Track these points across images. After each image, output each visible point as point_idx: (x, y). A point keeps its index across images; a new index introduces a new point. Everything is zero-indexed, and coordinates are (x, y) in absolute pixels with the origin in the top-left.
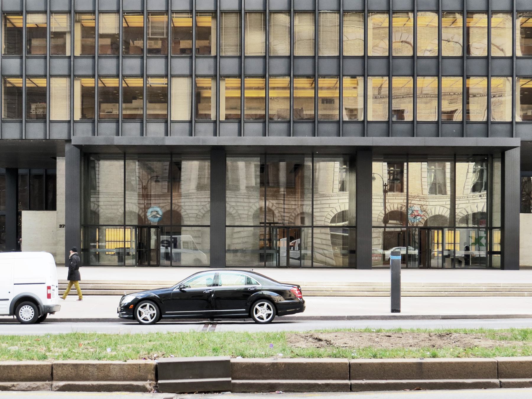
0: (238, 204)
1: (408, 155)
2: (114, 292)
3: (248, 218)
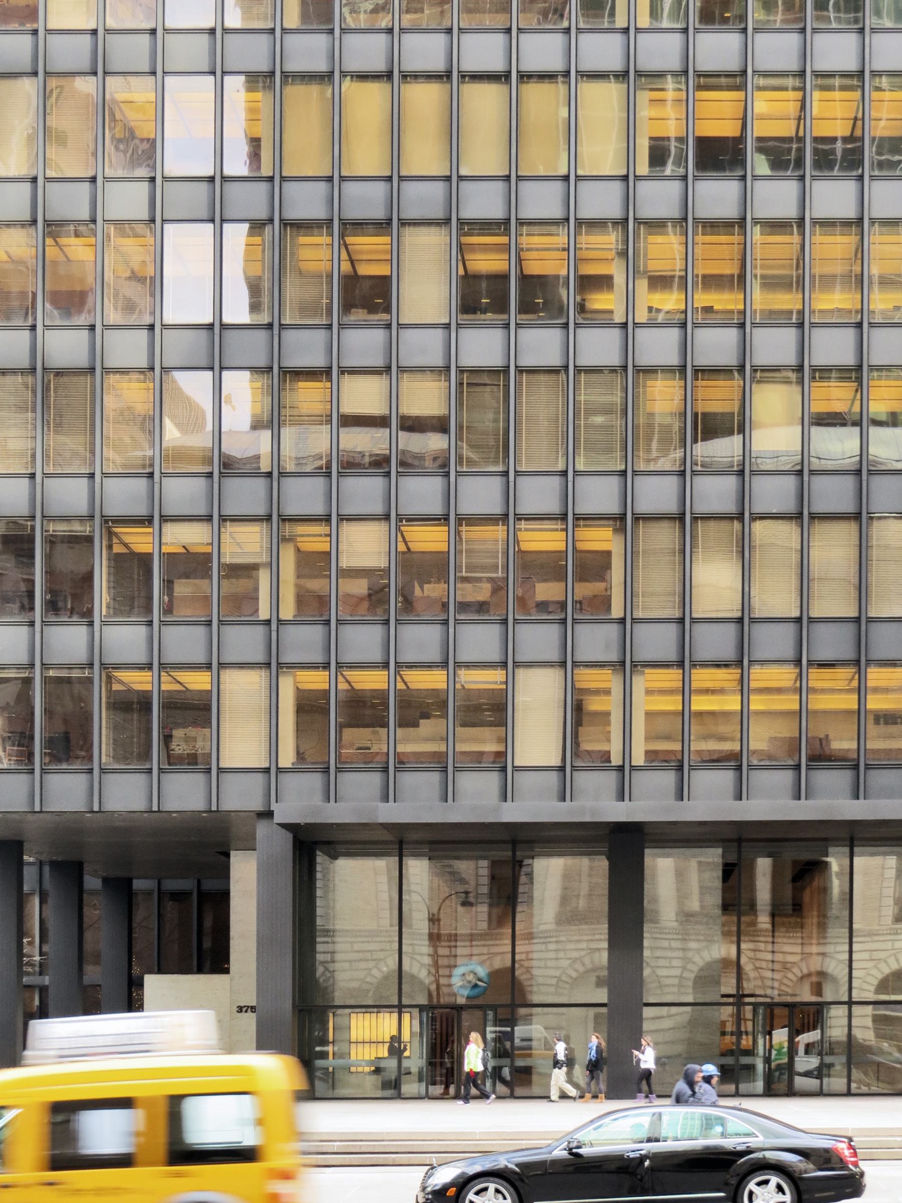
0: (659, 953)
2: (394, 1159)
3: (680, 986)
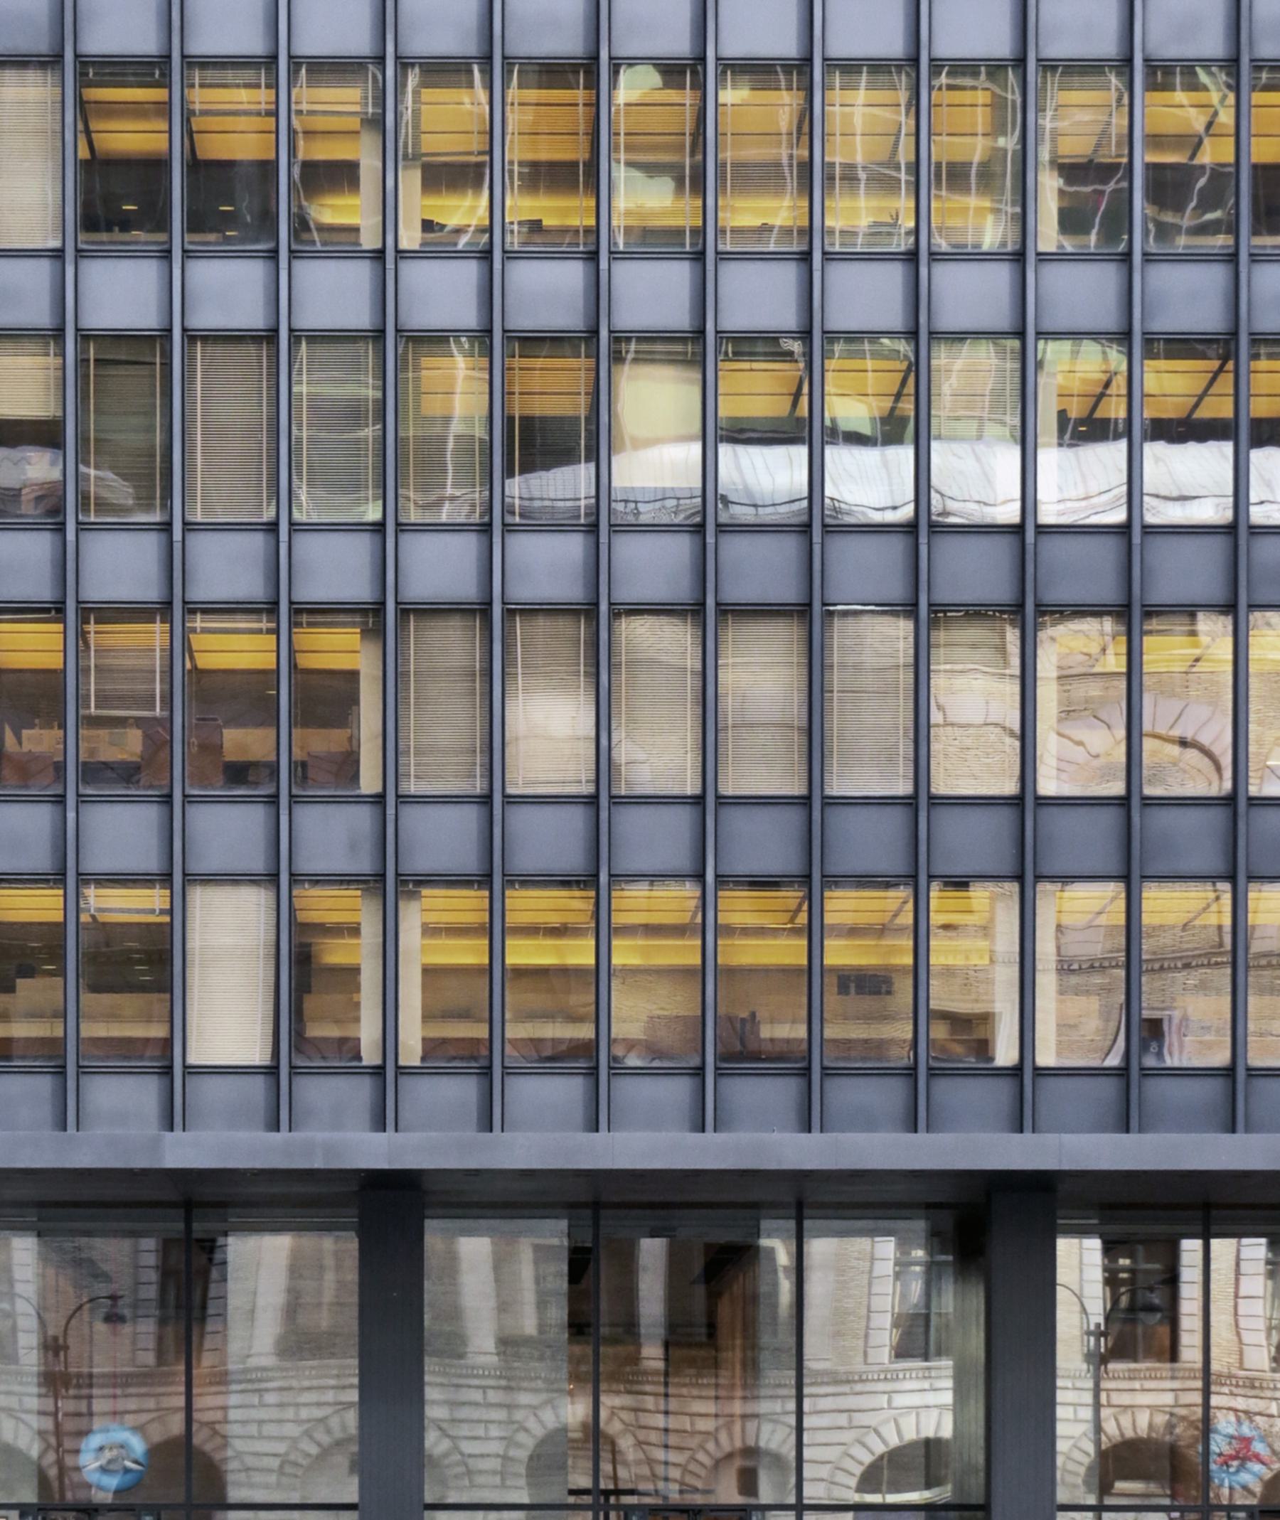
0: (464, 1413)
1: (1207, 1207)
